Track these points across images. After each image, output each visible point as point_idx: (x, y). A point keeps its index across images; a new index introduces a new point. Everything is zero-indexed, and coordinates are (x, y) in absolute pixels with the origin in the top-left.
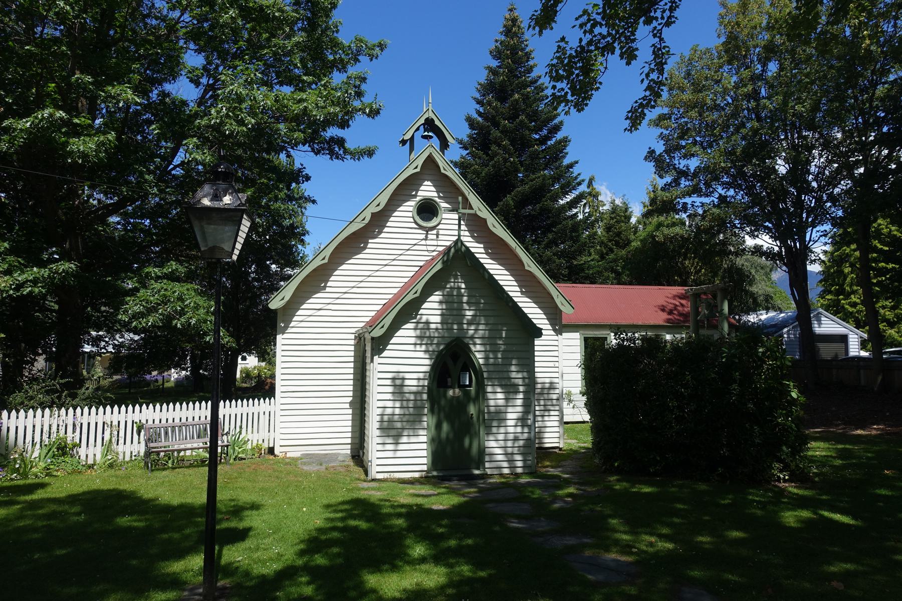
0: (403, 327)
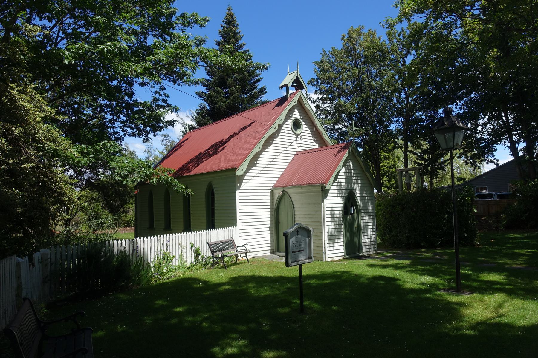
0: (251, 169)
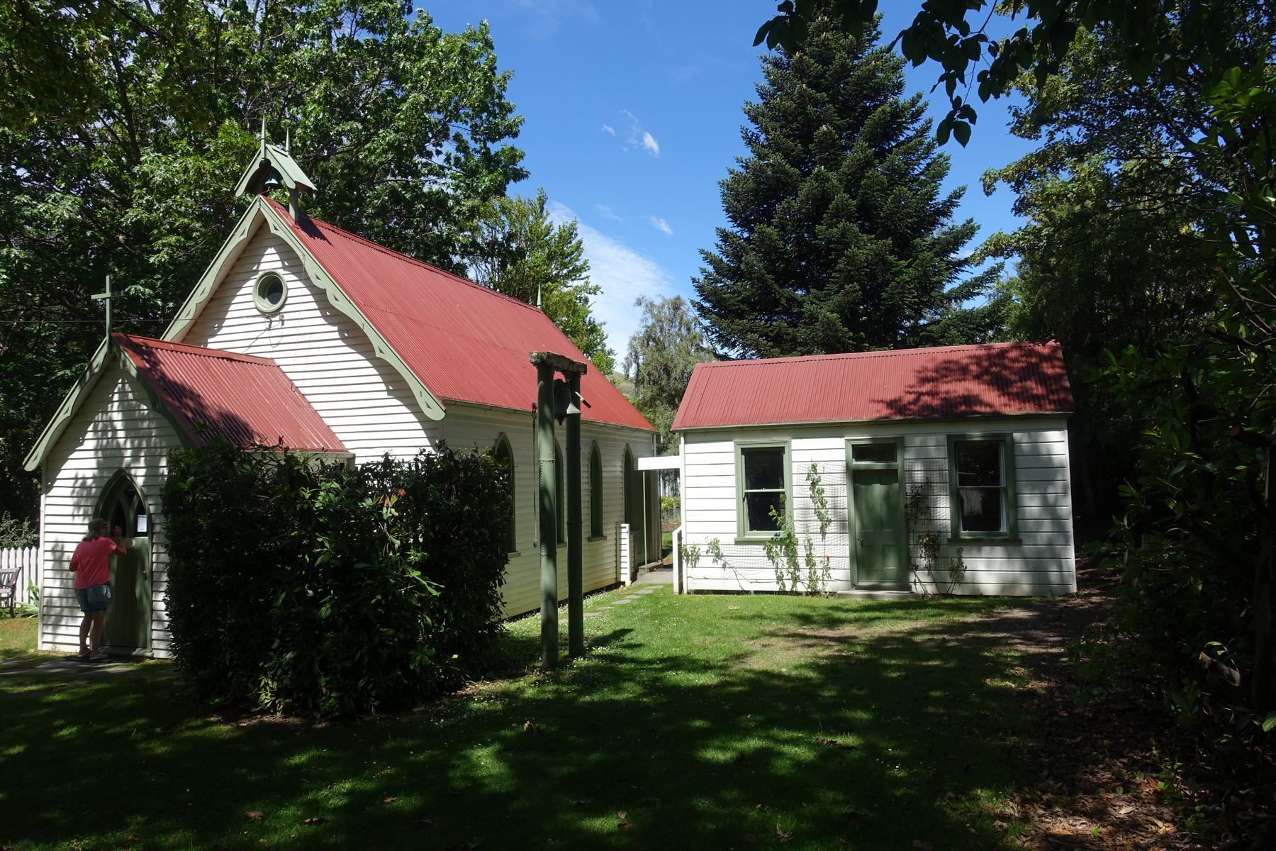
0: (70, 457)
